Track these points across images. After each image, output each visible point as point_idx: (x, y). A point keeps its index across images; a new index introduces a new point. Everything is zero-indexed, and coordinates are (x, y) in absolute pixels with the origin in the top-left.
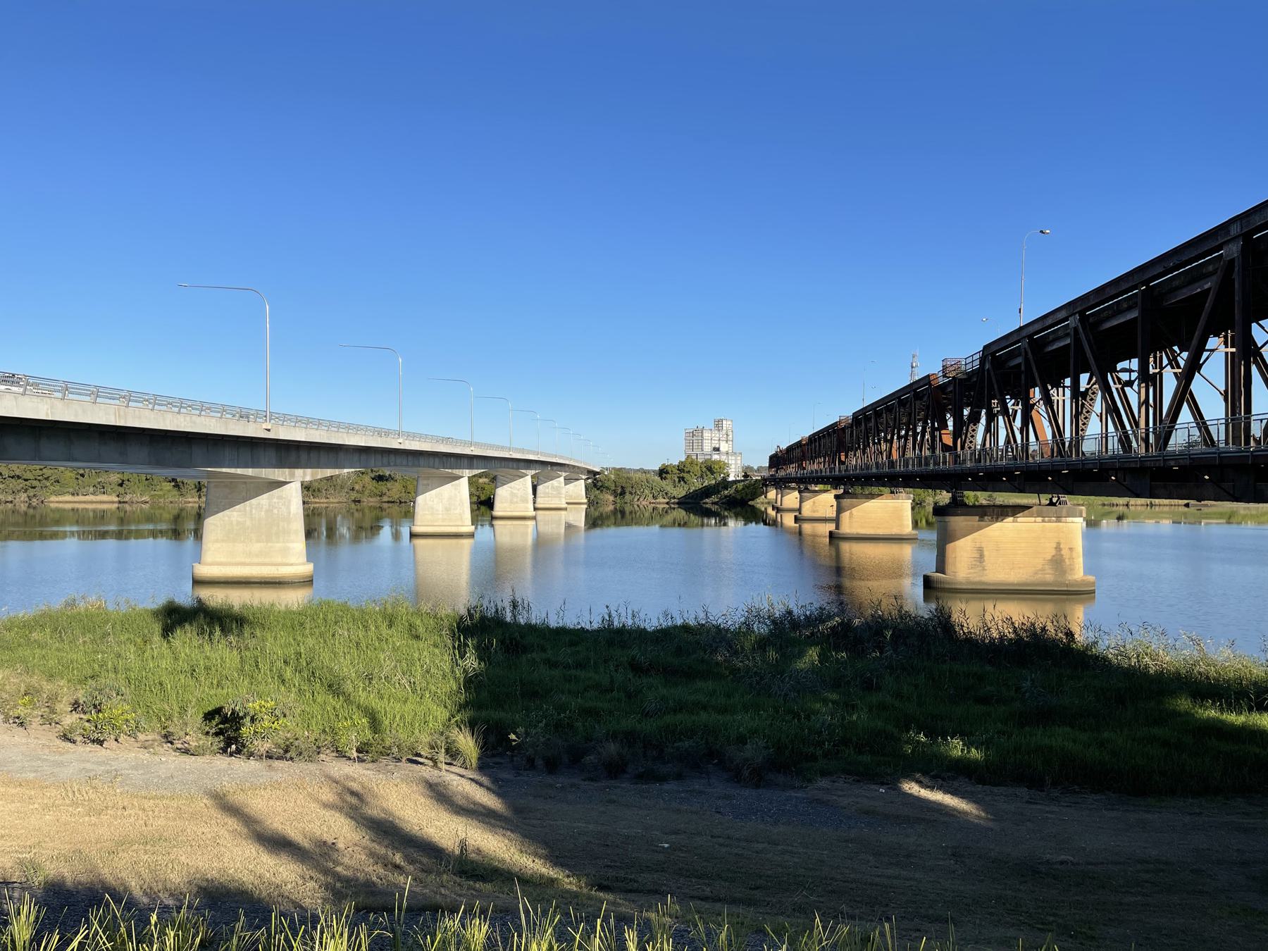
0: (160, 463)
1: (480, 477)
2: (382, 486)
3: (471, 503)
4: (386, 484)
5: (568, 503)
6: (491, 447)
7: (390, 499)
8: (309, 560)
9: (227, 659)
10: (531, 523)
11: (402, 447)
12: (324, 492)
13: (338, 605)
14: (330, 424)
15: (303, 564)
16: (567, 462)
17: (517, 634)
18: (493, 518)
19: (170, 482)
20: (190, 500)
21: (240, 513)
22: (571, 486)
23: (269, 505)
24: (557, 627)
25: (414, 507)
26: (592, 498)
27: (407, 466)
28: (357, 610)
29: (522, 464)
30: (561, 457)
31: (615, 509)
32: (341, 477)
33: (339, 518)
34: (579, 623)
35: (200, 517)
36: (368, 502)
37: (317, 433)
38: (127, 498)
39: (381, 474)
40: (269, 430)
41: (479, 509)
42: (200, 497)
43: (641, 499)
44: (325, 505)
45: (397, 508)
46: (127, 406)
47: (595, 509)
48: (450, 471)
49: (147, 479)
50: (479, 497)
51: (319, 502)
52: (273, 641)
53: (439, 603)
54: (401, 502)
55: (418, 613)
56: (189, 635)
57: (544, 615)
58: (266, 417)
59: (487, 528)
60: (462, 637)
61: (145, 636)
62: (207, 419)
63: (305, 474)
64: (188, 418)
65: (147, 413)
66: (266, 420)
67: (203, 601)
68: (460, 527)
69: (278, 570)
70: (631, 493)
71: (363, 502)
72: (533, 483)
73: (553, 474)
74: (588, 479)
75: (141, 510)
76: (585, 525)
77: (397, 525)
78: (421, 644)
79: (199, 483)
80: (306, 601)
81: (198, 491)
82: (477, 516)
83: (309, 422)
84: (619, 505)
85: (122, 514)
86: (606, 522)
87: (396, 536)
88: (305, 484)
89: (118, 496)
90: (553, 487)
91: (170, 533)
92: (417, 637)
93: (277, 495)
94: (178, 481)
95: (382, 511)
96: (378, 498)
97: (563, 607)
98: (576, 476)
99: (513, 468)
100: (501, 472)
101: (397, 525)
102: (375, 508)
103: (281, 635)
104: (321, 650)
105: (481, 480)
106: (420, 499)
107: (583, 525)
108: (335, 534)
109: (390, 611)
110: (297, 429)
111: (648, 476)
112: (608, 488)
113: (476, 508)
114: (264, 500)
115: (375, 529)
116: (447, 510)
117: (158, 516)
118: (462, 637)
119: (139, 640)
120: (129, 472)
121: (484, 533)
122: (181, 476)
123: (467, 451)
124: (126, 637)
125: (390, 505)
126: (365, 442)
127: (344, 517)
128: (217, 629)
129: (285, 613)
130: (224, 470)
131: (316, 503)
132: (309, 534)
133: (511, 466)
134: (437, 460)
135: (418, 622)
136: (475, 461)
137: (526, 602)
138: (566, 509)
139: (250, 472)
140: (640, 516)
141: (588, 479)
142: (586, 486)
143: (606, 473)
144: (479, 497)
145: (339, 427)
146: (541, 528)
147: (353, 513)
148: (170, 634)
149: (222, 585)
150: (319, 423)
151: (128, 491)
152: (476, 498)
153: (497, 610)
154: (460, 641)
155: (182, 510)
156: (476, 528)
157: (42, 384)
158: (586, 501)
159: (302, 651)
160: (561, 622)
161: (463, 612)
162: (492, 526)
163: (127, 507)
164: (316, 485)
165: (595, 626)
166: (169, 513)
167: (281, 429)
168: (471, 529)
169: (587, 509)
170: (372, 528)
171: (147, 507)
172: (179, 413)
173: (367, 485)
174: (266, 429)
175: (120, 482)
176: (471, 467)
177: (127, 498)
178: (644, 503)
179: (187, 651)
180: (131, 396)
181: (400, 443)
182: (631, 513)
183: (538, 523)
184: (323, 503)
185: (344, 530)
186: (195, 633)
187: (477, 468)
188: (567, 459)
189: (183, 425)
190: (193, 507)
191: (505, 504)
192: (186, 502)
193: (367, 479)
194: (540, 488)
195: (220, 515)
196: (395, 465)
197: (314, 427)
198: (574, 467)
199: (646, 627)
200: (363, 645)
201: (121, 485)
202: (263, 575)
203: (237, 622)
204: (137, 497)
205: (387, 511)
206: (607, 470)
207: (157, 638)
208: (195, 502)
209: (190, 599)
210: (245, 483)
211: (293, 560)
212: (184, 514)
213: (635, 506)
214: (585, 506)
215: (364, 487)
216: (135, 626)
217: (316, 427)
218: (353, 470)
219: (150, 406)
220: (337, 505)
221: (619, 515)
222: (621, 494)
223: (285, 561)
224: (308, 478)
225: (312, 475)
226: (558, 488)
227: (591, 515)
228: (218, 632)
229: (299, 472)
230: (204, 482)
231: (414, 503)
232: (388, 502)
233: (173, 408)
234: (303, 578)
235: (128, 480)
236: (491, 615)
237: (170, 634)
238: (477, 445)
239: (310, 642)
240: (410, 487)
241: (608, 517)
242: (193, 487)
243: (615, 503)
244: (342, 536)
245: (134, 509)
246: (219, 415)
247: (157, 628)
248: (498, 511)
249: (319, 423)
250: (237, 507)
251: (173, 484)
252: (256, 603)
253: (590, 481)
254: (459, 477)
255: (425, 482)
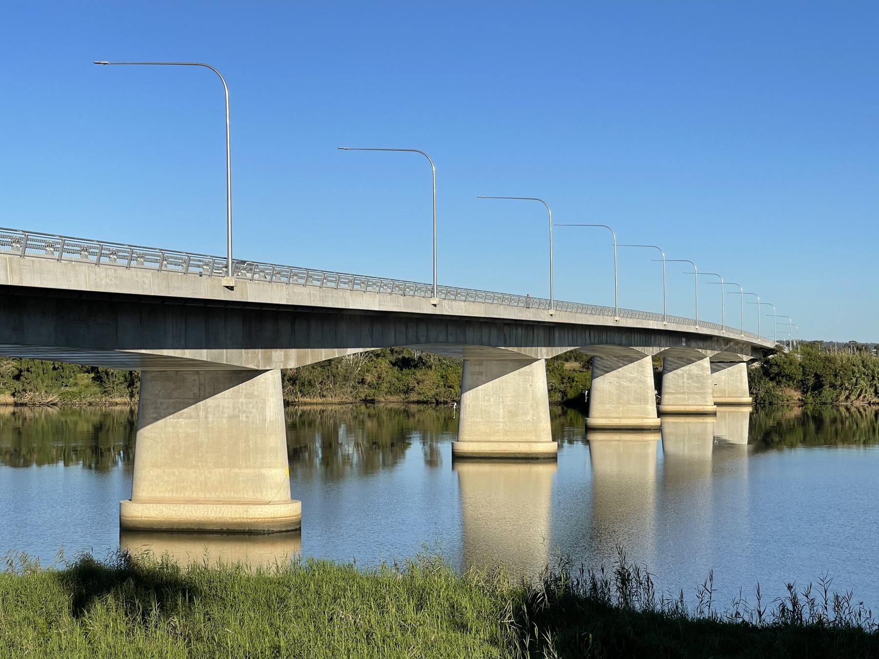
0: (72, 343)
1: (567, 360)
2: (409, 377)
3: (551, 404)
4: (414, 374)
5: (717, 404)
6: (582, 308)
7: (422, 398)
8: (295, 496)
9: (169, 654)
10: (654, 438)
11: (437, 311)
12: (318, 386)
13: (339, 569)
14: (324, 277)
15: (285, 502)
16: (716, 333)
17: (629, 628)
18: (589, 429)
19: (88, 372)
20: (118, 400)
21: (190, 421)
22: (724, 374)
23: (234, 408)
24: (699, 620)
25: (458, 410)
26: (762, 394)
27: (447, 342)
28: (367, 579)
29: (637, 337)
30: (703, 324)
31: (804, 414)
32: (344, 361)
33: (342, 431)
34: (738, 613)
35: (132, 427)
36: (387, 402)
37: (305, 291)
38: (27, 398)
39: (407, 357)
40: (231, 288)
41: (564, 413)
42: (132, 396)
43: (853, 397)
44: (320, 407)
45: (432, 412)
46: (23, 256)
47: (767, 415)
48: (515, 349)
49: (54, 369)
50: (564, 393)
51: (311, 403)
52: (238, 627)
53: (497, 570)
54: (438, 403)
55: (464, 585)
56: (113, 614)
57: (677, 597)
58: (226, 267)
59: (579, 446)
60: (536, 629)
61: (48, 614)
62: (140, 273)
63: (287, 358)
64: (111, 272)
65: (51, 264)
66: (227, 272)
67: (134, 560)
68: (533, 444)
69: (247, 511)
70: (833, 386)
71: (379, 402)
72: (655, 369)
73: (690, 353)
74: (753, 361)
75: (46, 416)
76: (749, 443)
77: (431, 441)
78: (469, 638)
79: (131, 373)
80: (288, 562)
81: (128, 387)
82: (563, 425)
83: (291, 274)
84: (810, 407)
85: (19, 423)
86: (788, 438)
87: (432, 461)
88: (289, 372)
89: (13, 395)
90: (690, 377)
91: (88, 451)
92: (463, 627)
93: (244, 392)
94: (100, 370)
95: (408, 416)
96: (403, 396)
97: (709, 583)
98: (730, 357)
99: (620, 345)
100: (603, 352)
101: (431, 441)
102: (397, 412)
103: (250, 617)
104: (312, 643)
105: (568, 366)
106: (469, 398)
107: (745, 441)
108: (336, 454)
109: (419, 581)
110: (275, 285)
111: (865, 355)
112: (790, 378)
113: (560, 412)
114: (225, 399)
115: (400, 442)
116: (513, 414)
117: (71, 426)
118: (536, 629)
119: (41, 621)
120: (30, 357)
121: (575, 452)
122: (103, 363)
123: (544, 316)
124: (23, 613)
125: (422, 407)
126: (485, 313)
127: (349, 431)
128: (155, 605)
129: (257, 581)
130: (166, 352)
131: (306, 404)
132: (295, 455)
133: (617, 340)
134: (494, 332)
135: (465, 602)
136: (557, 334)
137: (642, 575)
138: (714, 414)
139: (203, 354)
140: (850, 427)
141: (753, 361)
142: (749, 375)
143: (786, 351)
144: (564, 393)
145: (338, 281)
146: (671, 448)
147: (363, 422)
148: (86, 613)
149: (164, 535)
150: (309, 276)
151: (28, 387)
152: (560, 395)
153: (594, 585)
154: (533, 635)
155: (105, 415)
156: (560, 446)
157: (172, 258)
158: (749, 399)
159: (282, 644)
160: (706, 610)
161: (539, 586)
162: (587, 442)
163: (26, 410)
164: (305, 374)
165: (769, 619)
166: (87, 421)
167: (250, 286)
168: (551, 447)
169: (751, 414)
170: (392, 445)
171: (55, 412)
172: (98, 264)
173: (384, 375)
174: (227, 287)
175: (16, 372)
176: (550, 343)
177: (27, 398)
178: (858, 403)
179: (110, 640)
180: (28, 239)
181: (435, 305)
182: (834, 421)
183: (666, 438)
184: (316, 404)
185: (349, 449)
186: (122, 611)
187: (561, 345)
188: (715, 326)
189: (103, 282)
190: (122, 412)
191: (608, 406)
192: (112, 404)
193: (384, 364)
194: (669, 379)
195: (160, 422)
196: (428, 342)
197: (300, 281)
198: (727, 341)
199: (863, 625)
200: (377, 636)
201: (17, 377)
202: (223, 520)
203: (184, 595)
204: (40, 397)
205: (417, 418)
206: (788, 345)
207: (66, 618)
208: (125, 404)
209: (114, 557)
210: (198, 372)
211: (269, 495)
212: (109, 422)
213: (842, 409)
214: (749, 409)
215: (379, 378)
216: (35, 598)
217: (303, 281)
218: (361, 350)
219: (57, 254)
220: (337, 407)
221: (812, 426)
222: (814, 388)
223: (258, 496)
224: (292, 365)
225: (299, 358)
226: (699, 378)
227: (760, 425)
228: (155, 612)
229: (278, 354)
230: (138, 371)
231: (459, 403)
232: (418, 402)
233: (299, 280)
234: (286, 525)
235: (28, 370)
236: (585, 593)
237: (86, 613)
238: (561, 305)
239: (296, 629)
240: (453, 378)
241: (791, 430)
242: (122, 379)
243: (803, 403)
244: (347, 459)
245: (37, 415)
246: (157, 266)
247: (65, 600)
248: (597, 418)
249: (309, 276)
250: (185, 410)
251: (93, 375)
252: (213, 565)
253: (756, 365)
254: (530, 361)
255: (477, 369)
